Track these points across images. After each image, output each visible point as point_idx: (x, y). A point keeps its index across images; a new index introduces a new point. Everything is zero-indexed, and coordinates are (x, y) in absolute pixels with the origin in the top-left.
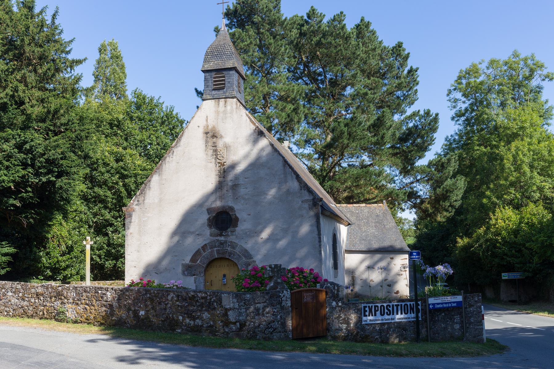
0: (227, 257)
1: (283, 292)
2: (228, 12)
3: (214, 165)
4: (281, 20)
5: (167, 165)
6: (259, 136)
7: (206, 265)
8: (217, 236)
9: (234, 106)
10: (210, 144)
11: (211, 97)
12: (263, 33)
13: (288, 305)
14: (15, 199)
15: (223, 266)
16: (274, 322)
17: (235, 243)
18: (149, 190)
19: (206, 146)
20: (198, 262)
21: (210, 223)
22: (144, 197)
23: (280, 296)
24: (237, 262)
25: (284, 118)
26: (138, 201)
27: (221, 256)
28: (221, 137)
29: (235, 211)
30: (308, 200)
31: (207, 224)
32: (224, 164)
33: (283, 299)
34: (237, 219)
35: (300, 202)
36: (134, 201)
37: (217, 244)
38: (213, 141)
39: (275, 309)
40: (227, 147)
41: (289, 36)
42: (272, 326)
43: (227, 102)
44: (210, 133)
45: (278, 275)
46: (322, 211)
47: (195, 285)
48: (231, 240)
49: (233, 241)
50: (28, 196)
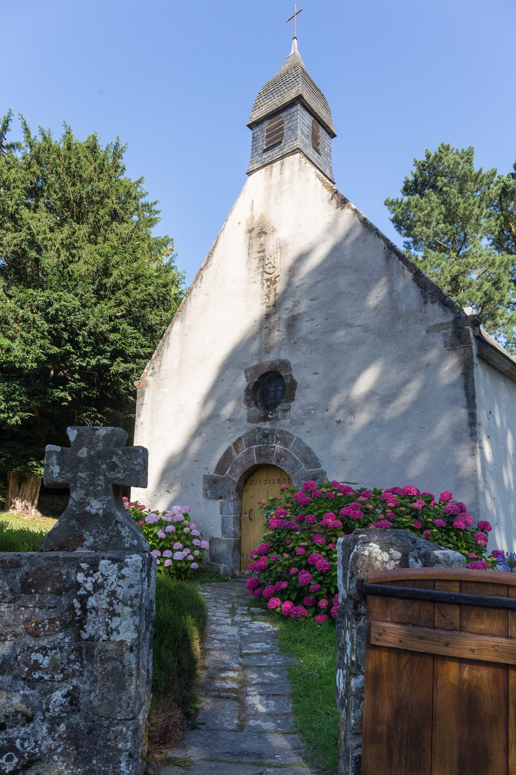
0: (274, 463)
1: (94, 566)
2: (406, 185)
3: (259, 285)
4: (473, 173)
5: (192, 301)
6: (339, 209)
7: (238, 478)
8: (259, 421)
9: (296, 167)
10: (256, 249)
11: (261, 165)
12: (447, 191)
13: (116, 637)
14: (62, 391)
15: (272, 482)
16: (29, 720)
17: (288, 433)
18: (168, 348)
19: (249, 254)
20: (227, 473)
21: (248, 398)
22: (160, 361)
23: (78, 586)
24: (290, 474)
25: (479, 298)
26: (153, 368)
27: (263, 461)
28: (274, 230)
29: (291, 369)
30: (442, 324)
31: (243, 399)
32: (275, 281)
33: (91, 602)
34: (294, 385)
35: (424, 332)
36: (148, 369)
37: (257, 438)
38: (260, 243)
39: (44, 650)
40: (281, 248)
41: (486, 194)
42: (11, 741)
43: (285, 164)
44: (256, 230)
45: (94, 476)
46: (479, 349)
47: (220, 516)
48: (281, 428)
49: (285, 429)
50: (78, 386)
